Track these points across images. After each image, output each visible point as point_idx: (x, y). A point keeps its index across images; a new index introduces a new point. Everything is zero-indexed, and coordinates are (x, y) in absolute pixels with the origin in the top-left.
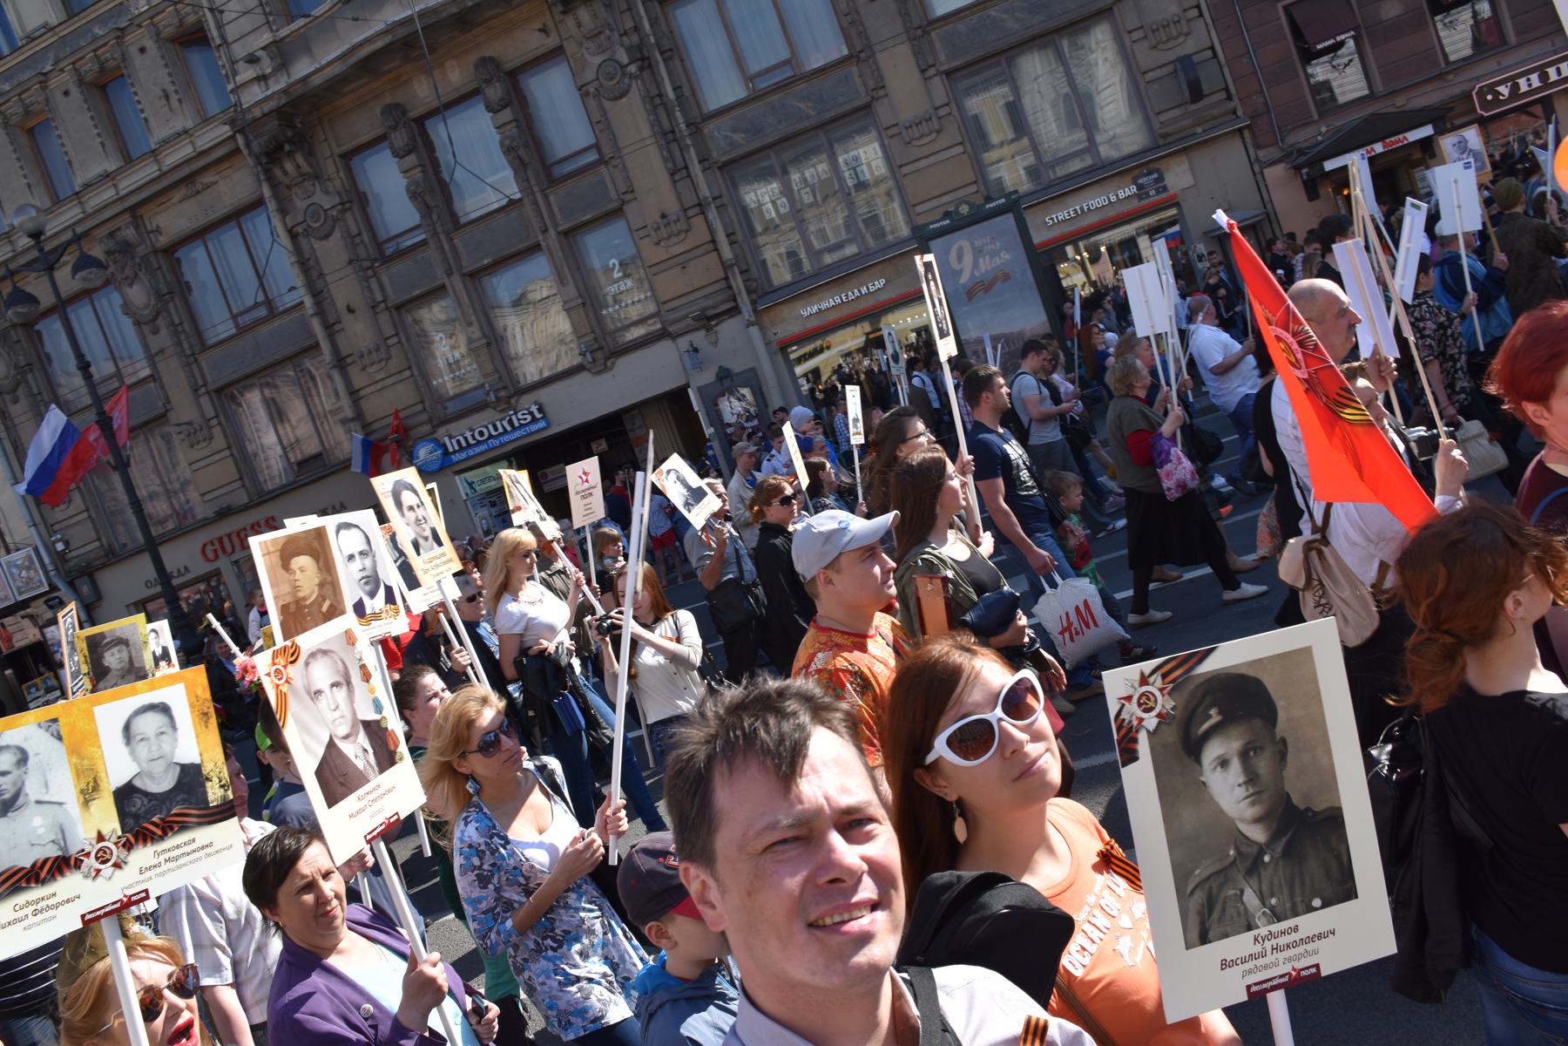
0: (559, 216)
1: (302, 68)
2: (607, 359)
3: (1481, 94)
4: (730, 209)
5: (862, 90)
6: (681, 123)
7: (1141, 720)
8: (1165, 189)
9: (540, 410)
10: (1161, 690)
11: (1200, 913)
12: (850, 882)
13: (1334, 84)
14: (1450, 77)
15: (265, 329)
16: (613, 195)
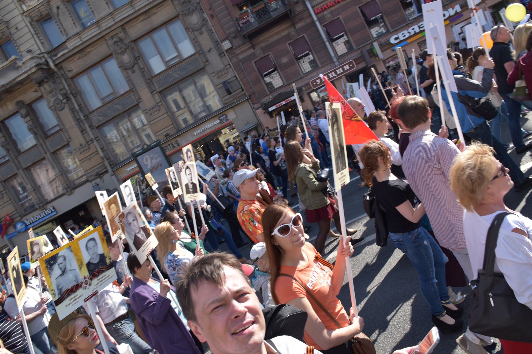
0: (50, 148)
2: (71, 190)
3: (312, 83)
4: (102, 141)
6: (84, 116)
8: (228, 120)
9: (54, 208)
12: (242, 316)
13: (273, 82)
14: (304, 78)
16: (65, 140)
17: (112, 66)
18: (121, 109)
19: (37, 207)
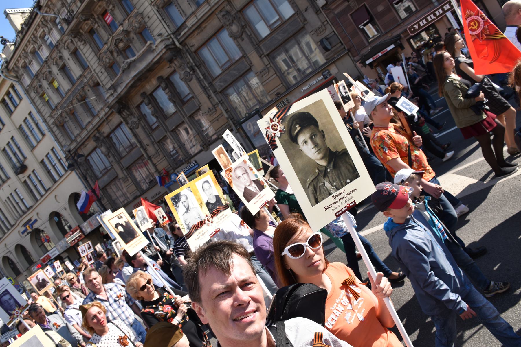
1: (119, 90)
2: (207, 147)
5: (247, 65)
7: (275, 134)
8: (331, 74)
9: (196, 162)
10: (278, 123)
11: (313, 194)
14: (402, 24)
15: (132, 152)
17: (225, 35)
18: (238, 73)
19: (184, 161)
